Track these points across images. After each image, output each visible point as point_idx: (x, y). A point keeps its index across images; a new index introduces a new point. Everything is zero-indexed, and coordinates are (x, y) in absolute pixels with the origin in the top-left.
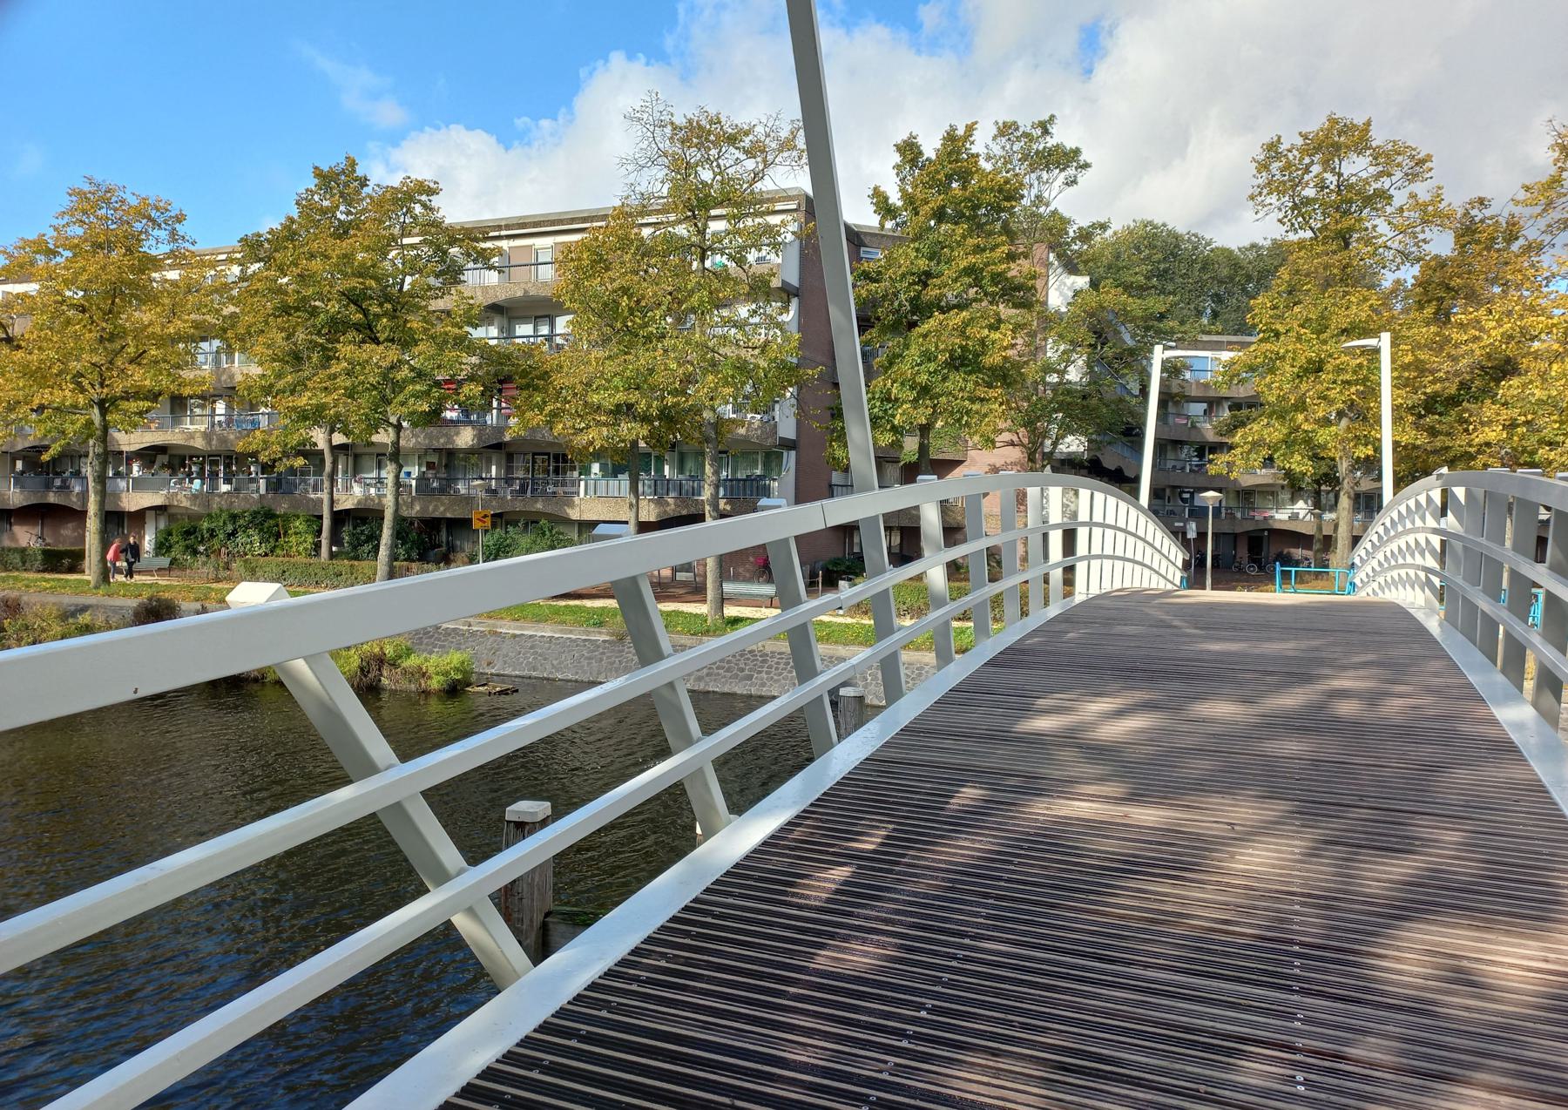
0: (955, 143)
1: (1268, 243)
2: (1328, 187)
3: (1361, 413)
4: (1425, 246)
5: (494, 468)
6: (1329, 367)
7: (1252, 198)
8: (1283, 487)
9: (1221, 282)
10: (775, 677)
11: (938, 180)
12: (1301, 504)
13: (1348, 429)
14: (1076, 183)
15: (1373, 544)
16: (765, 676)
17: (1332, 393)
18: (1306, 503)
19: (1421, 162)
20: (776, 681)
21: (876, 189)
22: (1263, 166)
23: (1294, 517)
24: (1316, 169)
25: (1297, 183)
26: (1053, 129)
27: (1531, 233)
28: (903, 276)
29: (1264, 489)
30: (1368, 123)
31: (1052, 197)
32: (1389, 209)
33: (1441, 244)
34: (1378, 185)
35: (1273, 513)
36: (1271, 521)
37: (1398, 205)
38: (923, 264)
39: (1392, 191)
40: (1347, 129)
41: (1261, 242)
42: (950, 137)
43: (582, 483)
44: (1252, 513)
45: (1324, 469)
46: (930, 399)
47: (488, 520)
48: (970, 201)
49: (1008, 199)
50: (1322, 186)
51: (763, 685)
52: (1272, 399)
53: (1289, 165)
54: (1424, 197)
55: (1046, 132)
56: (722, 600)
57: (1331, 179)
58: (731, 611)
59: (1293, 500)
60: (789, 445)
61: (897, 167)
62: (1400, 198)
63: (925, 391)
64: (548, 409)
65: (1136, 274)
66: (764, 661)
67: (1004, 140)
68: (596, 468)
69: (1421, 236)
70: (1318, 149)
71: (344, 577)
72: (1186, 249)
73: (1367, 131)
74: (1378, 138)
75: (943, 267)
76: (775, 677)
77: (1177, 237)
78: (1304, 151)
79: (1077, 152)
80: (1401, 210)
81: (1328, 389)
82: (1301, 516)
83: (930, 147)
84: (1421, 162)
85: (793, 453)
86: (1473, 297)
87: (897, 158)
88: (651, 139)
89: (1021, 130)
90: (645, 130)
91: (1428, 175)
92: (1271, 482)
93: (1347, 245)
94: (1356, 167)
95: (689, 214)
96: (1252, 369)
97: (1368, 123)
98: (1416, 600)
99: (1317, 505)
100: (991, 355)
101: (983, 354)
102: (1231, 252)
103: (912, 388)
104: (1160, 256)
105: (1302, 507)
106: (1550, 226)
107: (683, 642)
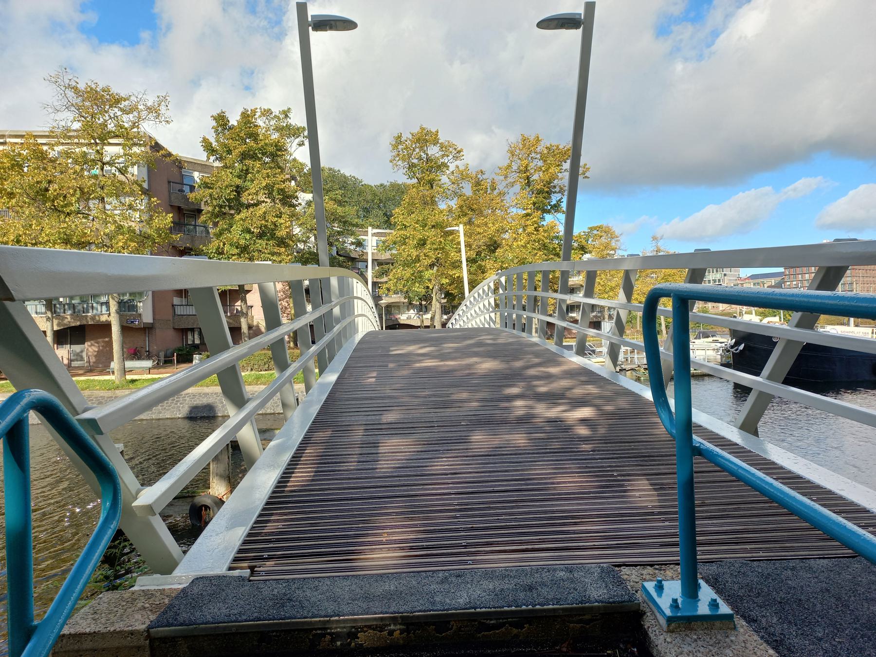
0: (247, 117)
1: (388, 184)
2: (422, 159)
4: (462, 190)
6: (428, 242)
7: (391, 161)
9: (368, 202)
10: (167, 408)
11: (241, 137)
13: (438, 270)
14: (304, 145)
15: (468, 318)
16: (161, 408)
17: (430, 254)
19: (459, 152)
20: (168, 410)
23: (409, 318)
24: (417, 150)
26: (291, 115)
27: (501, 187)
28: (227, 187)
29: (394, 305)
33: (468, 190)
36: (399, 320)
37: (451, 170)
38: (238, 182)
39: (448, 164)
40: (428, 133)
41: (386, 183)
46: (247, 254)
48: (261, 150)
49: (280, 150)
50: (420, 159)
51: (160, 413)
53: (407, 148)
54: (462, 168)
55: (287, 116)
56: (125, 371)
57: (424, 155)
58: (129, 377)
59: (408, 310)
62: (452, 167)
65: (337, 194)
67: (265, 118)
69: (461, 185)
72: (350, 184)
73: (437, 135)
74: (442, 138)
75: (248, 184)
76: (167, 408)
77: (345, 177)
80: (453, 172)
81: (429, 252)
82: (412, 317)
83: (234, 120)
84: (459, 152)
86: (481, 213)
87: (214, 123)
88: (63, 95)
89: (274, 114)
90: (59, 89)
91: (462, 158)
93: (432, 187)
94: (433, 151)
95: (93, 141)
96: (395, 243)
97: (437, 132)
100: (280, 231)
101: (275, 230)
102: (372, 187)
103: (237, 248)
105: (412, 313)
106: (507, 185)
107: (102, 395)
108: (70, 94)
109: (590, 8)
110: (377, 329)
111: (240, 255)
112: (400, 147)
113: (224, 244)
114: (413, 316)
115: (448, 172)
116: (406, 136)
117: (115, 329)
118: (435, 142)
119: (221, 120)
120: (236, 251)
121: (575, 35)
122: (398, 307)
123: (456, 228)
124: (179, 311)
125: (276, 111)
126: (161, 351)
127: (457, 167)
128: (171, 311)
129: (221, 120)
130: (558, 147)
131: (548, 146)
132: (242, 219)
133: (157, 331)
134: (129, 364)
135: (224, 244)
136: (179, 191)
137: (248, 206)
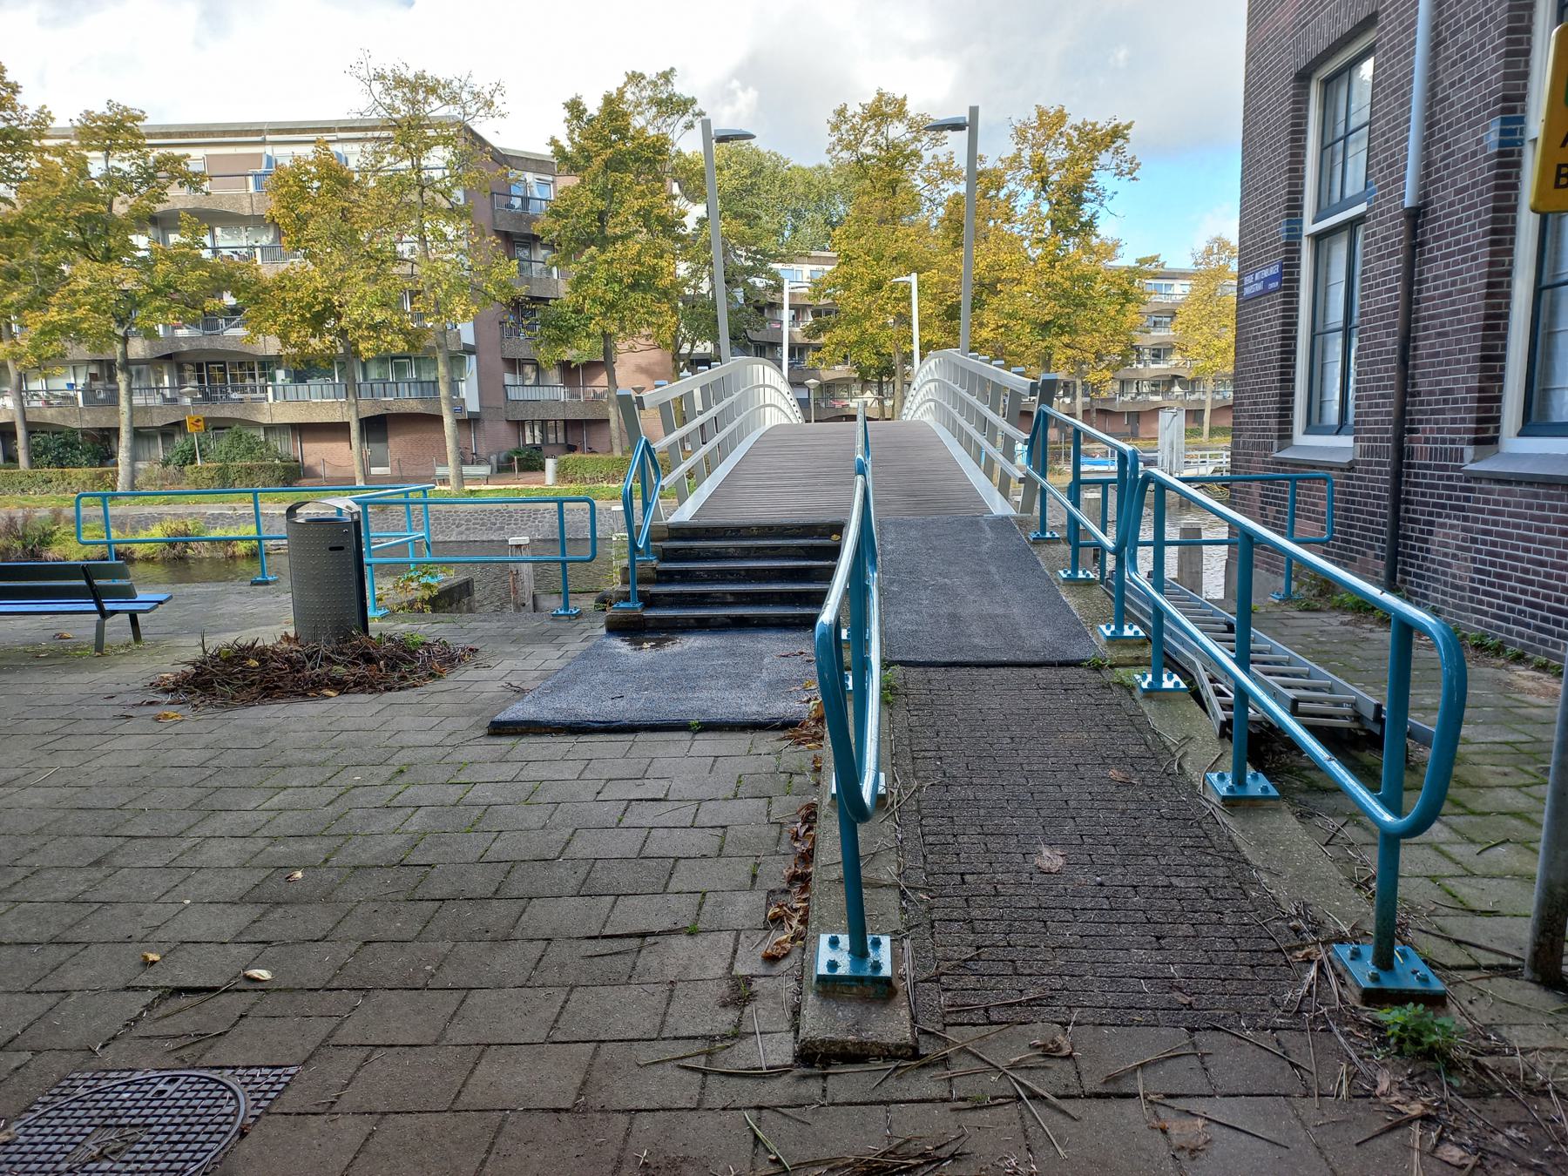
3: (904, 319)
5: (166, 378)
8: (855, 380)
12: (868, 394)
21: (552, 138)
22: (836, 127)
24: (871, 132)
25: (859, 141)
26: (674, 80)
30: (905, 98)
31: (1444, 818)
32: (921, 166)
34: (912, 147)
35: (846, 402)
38: (600, 204)
42: (608, 100)
43: (270, 389)
45: (884, 364)
47: (201, 424)
52: (848, 309)
55: (668, 81)
59: (863, 392)
60: (470, 350)
61: (566, 120)
62: (927, 157)
63: (612, 306)
64: (281, 320)
66: (512, 516)
68: (280, 375)
69: (942, 187)
70: (872, 117)
71: (54, 483)
74: (912, 109)
78: (864, 119)
79: (693, 101)
85: (474, 357)
97: (905, 98)
98: (929, 419)
99: (880, 392)
103: (602, 304)
104: (746, 172)
108: (377, 87)
109: (974, 111)
110: (795, 422)
111: (605, 314)
112: (844, 127)
113: (584, 299)
114: (870, 401)
115: (921, 166)
116: (854, 108)
117: (448, 421)
118: (901, 114)
119: (575, 108)
120: (598, 309)
121: (963, 135)
122: (848, 387)
123: (908, 279)
124: (513, 394)
125: (651, 73)
126: (491, 453)
127: (935, 157)
128: (502, 395)
129: (575, 108)
130: (1094, 125)
131: (1079, 124)
132: (606, 262)
133: (486, 423)
134: (467, 470)
135: (584, 299)
136: (507, 206)
137: (616, 238)
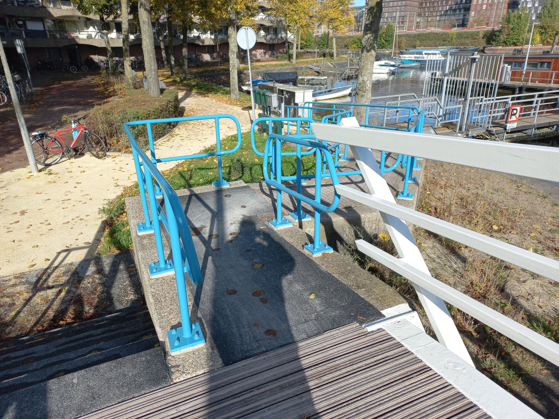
18: (94, 28)
23: (89, 37)
36: (77, 40)
44: (66, 35)
59: (88, 27)
92: (71, 14)
105: (92, 31)
